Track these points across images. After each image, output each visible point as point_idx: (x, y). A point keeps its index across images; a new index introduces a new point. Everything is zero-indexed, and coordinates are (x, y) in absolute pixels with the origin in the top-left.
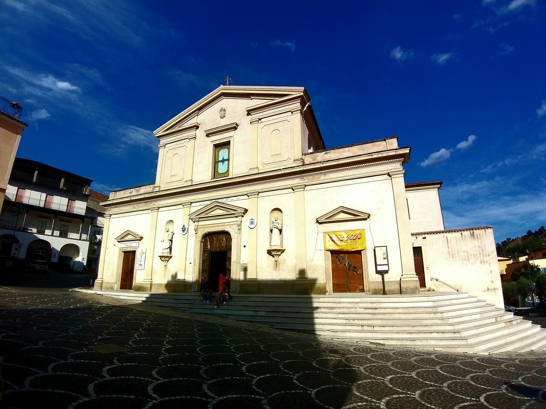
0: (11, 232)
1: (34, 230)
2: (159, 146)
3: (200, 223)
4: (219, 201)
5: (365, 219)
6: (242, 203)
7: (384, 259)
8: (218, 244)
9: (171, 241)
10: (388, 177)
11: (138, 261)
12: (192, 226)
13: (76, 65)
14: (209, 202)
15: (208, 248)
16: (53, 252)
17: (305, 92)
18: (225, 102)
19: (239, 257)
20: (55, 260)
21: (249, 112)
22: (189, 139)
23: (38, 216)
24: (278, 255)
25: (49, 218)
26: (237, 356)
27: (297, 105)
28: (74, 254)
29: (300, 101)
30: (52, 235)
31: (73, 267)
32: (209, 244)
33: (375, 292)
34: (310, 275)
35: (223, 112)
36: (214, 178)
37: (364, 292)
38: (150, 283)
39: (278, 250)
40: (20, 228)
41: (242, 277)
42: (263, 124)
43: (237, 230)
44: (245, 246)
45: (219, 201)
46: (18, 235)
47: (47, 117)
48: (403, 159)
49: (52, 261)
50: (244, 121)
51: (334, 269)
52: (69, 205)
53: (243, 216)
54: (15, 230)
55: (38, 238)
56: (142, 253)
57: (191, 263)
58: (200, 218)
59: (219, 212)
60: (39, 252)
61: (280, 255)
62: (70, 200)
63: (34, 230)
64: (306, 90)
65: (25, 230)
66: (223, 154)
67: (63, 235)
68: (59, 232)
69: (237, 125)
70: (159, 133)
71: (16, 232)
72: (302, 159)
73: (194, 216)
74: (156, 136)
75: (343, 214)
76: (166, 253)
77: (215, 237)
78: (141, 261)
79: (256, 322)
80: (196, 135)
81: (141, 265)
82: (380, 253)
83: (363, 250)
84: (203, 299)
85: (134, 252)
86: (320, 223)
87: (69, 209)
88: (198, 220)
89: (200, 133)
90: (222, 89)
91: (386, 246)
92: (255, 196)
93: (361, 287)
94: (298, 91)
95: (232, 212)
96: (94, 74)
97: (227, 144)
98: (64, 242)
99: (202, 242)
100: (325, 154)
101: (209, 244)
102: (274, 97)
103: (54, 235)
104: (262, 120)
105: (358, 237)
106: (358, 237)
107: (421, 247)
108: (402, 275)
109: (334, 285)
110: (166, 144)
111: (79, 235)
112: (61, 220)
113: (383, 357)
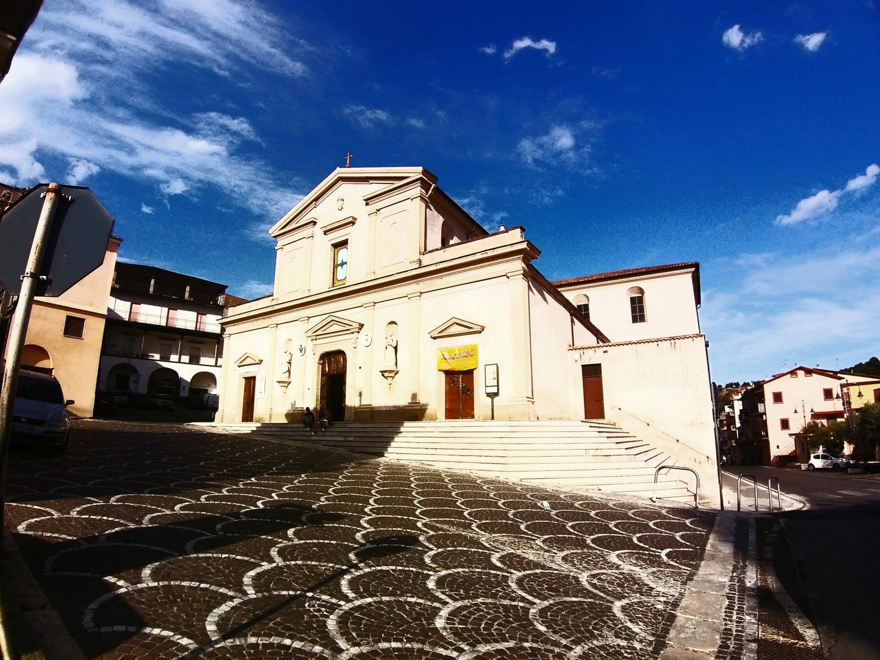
0: (125, 360)
1: (157, 357)
2: (276, 249)
3: (318, 342)
5: (480, 332)
6: (355, 316)
8: (335, 366)
9: (290, 363)
12: (309, 345)
13: (213, 114)
16: (182, 383)
17: (425, 172)
18: (345, 189)
20: (184, 393)
21: (368, 201)
22: (412, 199)
23: (160, 338)
24: (391, 377)
25: (174, 340)
27: (417, 190)
28: (209, 385)
29: (420, 184)
30: (179, 362)
31: (207, 402)
32: (327, 367)
34: (422, 400)
35: (341, 202)
36: (333, 286)
38: (269, 413)
39: (391, 371)
40: (138, 355)
41: (357, 405)
42: (382, 216)
44: (360, 368)
46: (134, 362)
47: (183, 192)
48: (522, 255)
49: (182, 395)
52: (199, 320)
53: (359, 332)
54: (130, 358)
55: (161, 366)
58: (316, 336)
59: (336, 328)
60: (169, 385)
61: (394, 377)
62: (200, 314)
63: (157, 357)
64: (427, 170)
65: (145, 357)
66: (343, 254)
67: (194, 360)
68: (188, 357)
69: (356, 219)
71: (131, 359)
74: (272, 236)
75: (456, 326)
76: (285, 377)
77: (333, 357)
80: (314, 233)
83: (475, 369)
84: (304, 426)
87: (198, 327)
88: (315, 338)
90: (339, 172)
91: (497, 364)
94: (415, 172)
95: (348, 327)
96: (240, 125)
97: (344, 244)
98: (195, 369)
99: (320, 364)
100: (444, 252)
101: (327, 367)
102: (394, 180)
103: (182, 361)
105: (471, 353)
106: (471, 353)
107: (600, 364)
109: (447, 410)
110: (284, 245)
111: (215, 360)
112: (190, 342)
113: (607, 516)
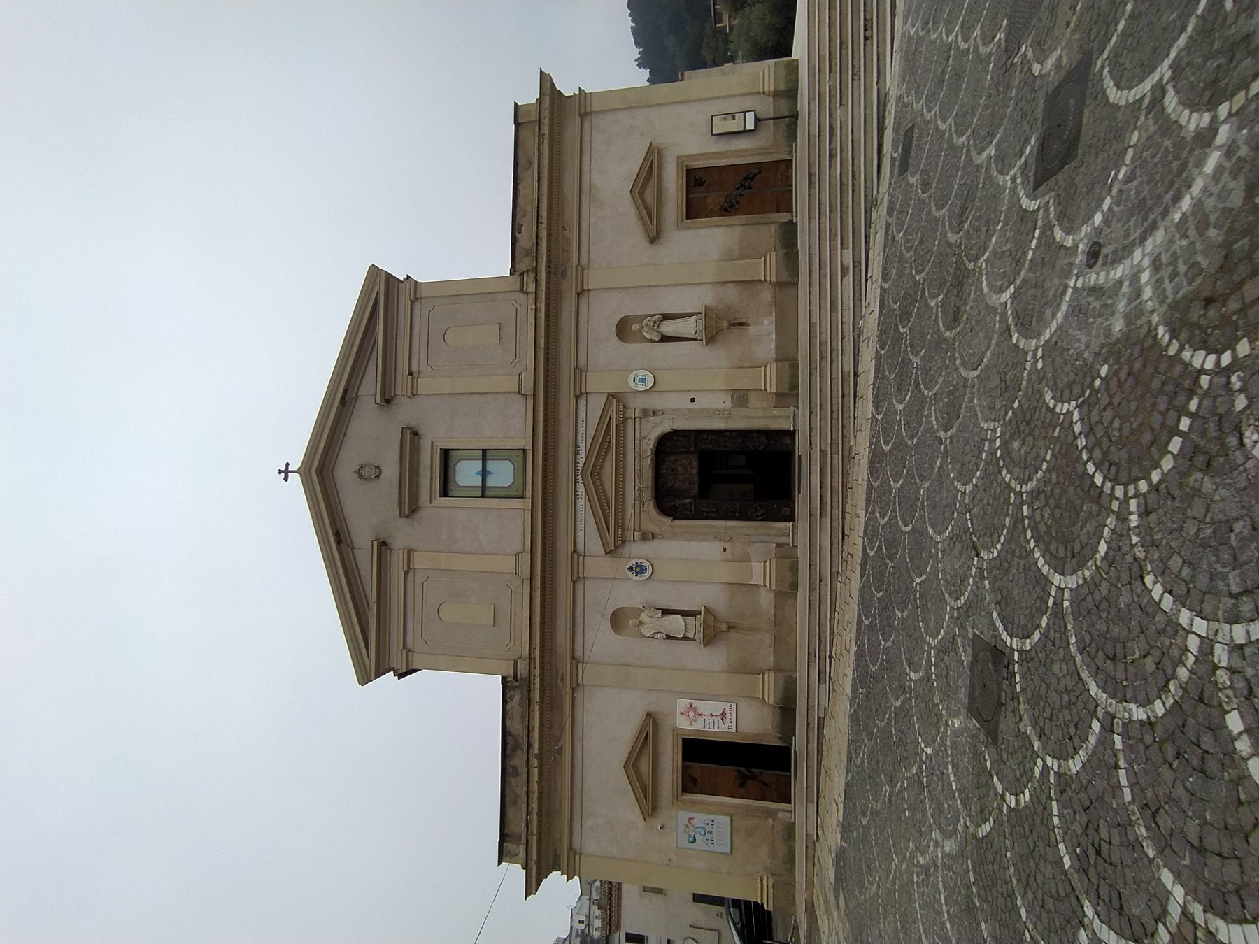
4: (580, 467)
6: (590, 414)
7: (734, 118)
10: (586, 295)
11: (711, 726)
14: (581, 488)
15: (690, 503)
19: (715, 413)
26: (900, 616)
33: (792, 134)
37: (792, 160)
42: (423, 367)
43: (657, 419)
44: (693, 400)
45: (580, 467)
50: (406, 412)
51: (755, 57)
56: (691, 714)
57: (725, 549)
70: (368, 664)
72: (522, 275)
73: (609, 539)
78: (712, 715)
79: (857, 349)
81: (723, 714)
82: (721, 126)
85: (687, 742)
86: (659, 233)
89: (403, 536)
92: (580, 669)
93: (782, 167)
104: (414, 368)
108: (764, 93)
